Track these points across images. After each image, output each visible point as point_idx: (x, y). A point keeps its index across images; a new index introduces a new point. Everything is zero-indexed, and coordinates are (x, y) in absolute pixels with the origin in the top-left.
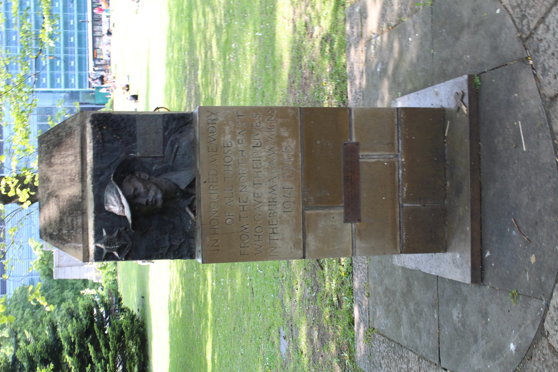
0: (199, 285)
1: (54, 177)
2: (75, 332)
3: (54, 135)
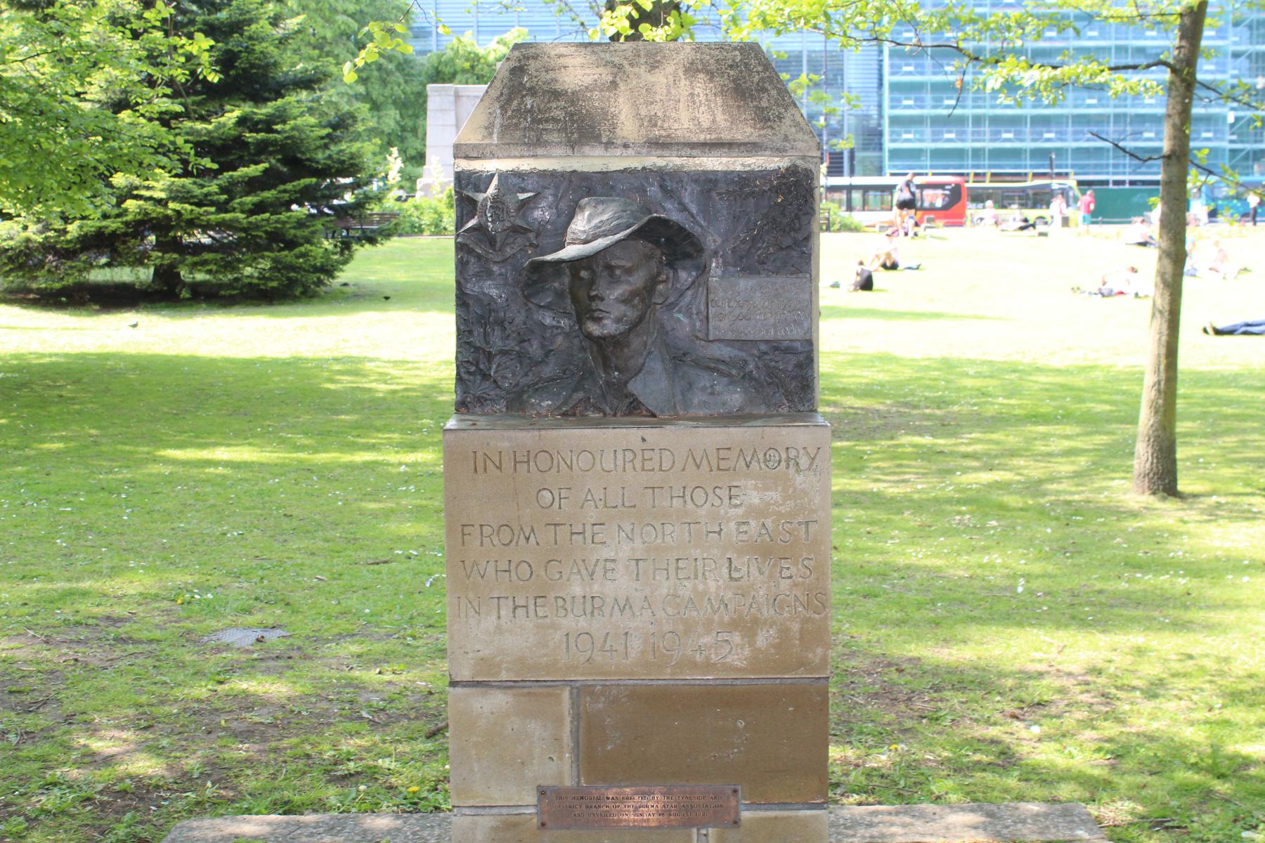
0: (402, 431)
1: (660, 79)
2: (295, 133)
3: (762, 79)
